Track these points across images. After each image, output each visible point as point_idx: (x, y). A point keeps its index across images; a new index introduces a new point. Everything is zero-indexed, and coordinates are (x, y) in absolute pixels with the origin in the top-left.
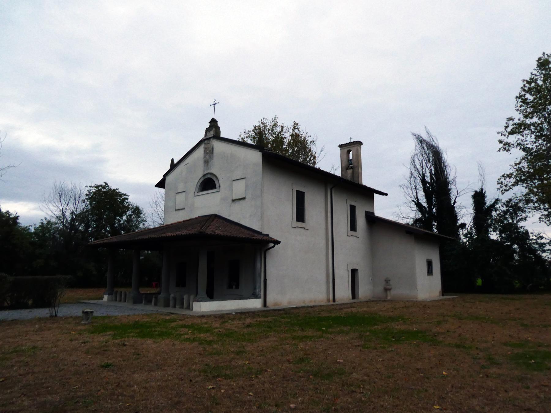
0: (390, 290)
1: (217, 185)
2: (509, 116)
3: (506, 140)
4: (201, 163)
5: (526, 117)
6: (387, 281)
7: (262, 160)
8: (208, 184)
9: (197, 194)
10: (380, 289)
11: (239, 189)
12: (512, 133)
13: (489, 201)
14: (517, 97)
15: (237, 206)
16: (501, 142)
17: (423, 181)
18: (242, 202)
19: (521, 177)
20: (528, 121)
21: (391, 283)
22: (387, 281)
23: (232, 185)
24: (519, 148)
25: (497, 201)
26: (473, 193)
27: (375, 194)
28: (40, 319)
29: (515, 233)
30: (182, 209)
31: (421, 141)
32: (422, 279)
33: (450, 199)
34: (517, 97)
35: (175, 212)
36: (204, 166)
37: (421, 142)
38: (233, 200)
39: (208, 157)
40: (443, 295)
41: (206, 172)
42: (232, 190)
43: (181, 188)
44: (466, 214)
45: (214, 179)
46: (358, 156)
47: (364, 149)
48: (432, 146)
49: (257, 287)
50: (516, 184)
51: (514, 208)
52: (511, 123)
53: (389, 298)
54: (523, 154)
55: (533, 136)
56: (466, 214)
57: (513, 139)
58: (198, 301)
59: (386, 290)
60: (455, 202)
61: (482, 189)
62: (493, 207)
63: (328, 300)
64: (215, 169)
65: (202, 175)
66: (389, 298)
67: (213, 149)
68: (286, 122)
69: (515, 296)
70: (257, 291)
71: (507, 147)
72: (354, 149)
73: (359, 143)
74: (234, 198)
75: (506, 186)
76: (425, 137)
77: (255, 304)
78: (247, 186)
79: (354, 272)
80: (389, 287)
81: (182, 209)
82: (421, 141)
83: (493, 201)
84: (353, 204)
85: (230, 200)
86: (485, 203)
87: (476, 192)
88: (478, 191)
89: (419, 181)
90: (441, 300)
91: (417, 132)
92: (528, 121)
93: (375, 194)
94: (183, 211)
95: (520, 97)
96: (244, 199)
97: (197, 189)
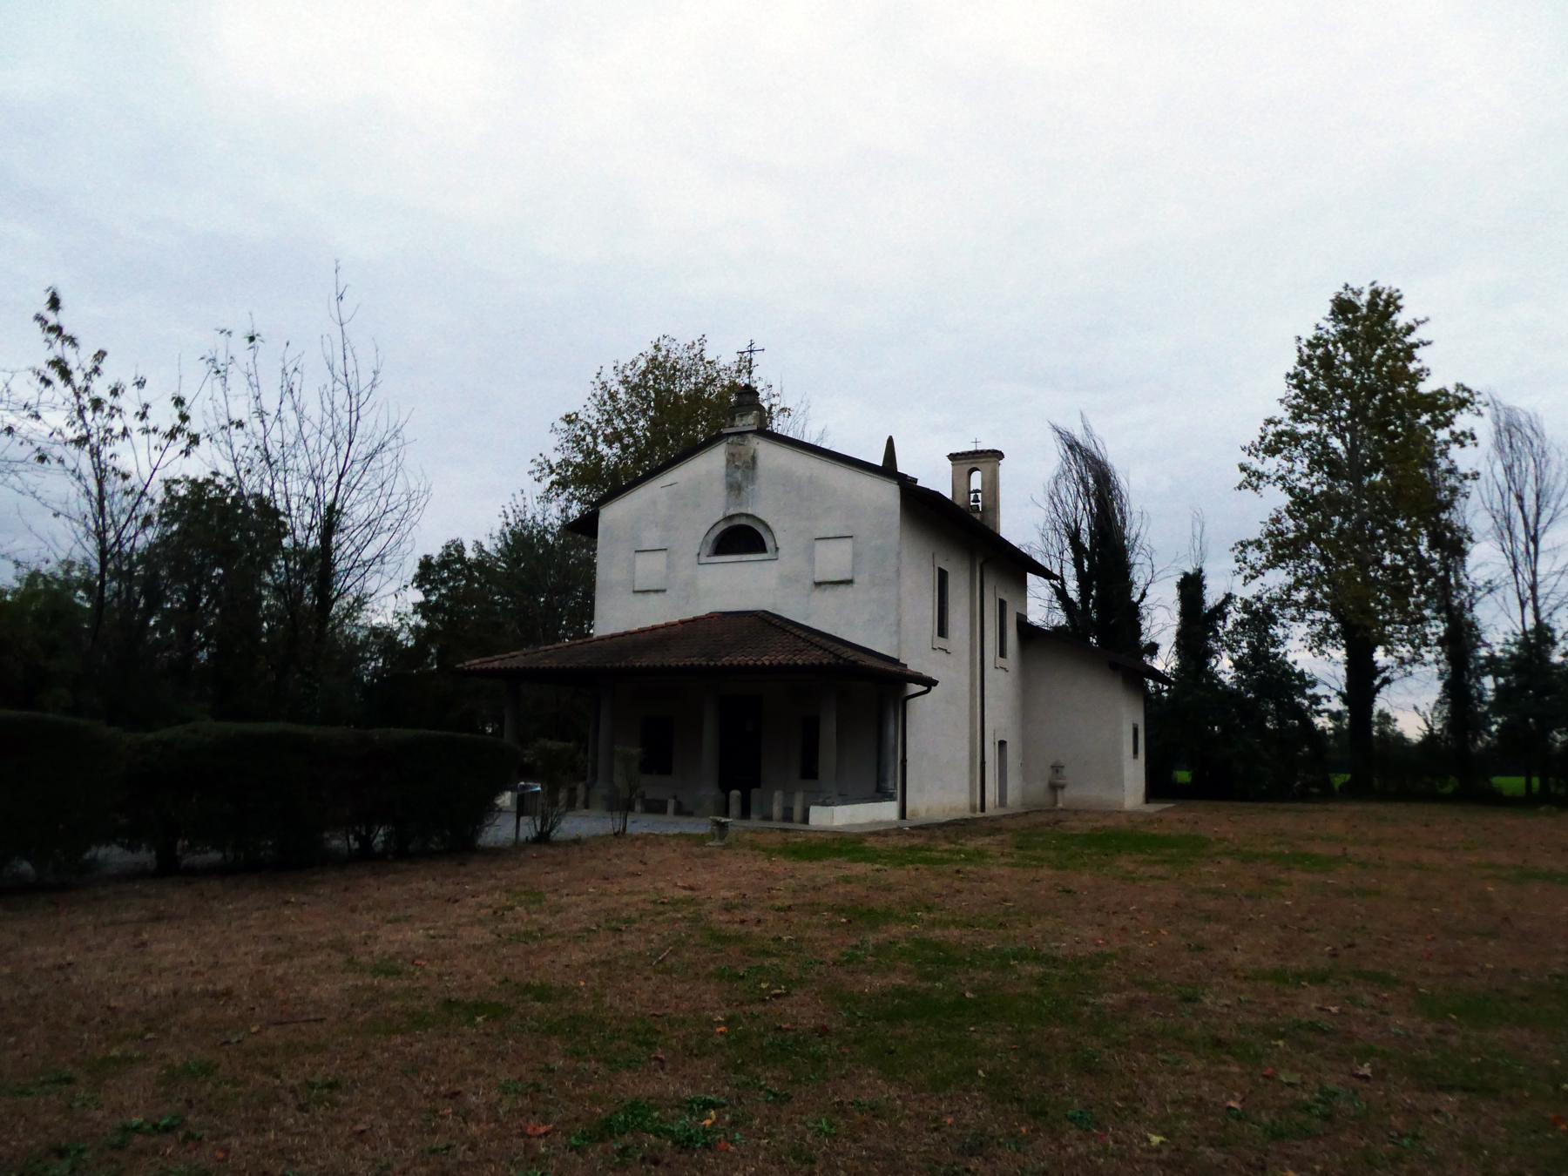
0: (1063, 787)
1: (769, 544)
2: (1268, 416)
3: (1255, 464)
4: (719, 488)
5: (1297, 417)
6: (1057, 768)
7: (898, 501)
8: (740, 538)
9: (704, 559)
10: (1039, 788)
11: (834, 560)
12: (1272, 450)
13: (1212, 597)
14: (1288, 375)
15: (830, 597)
16: (1243, 468)
17: (1074, 537)
18: (842, 588)
19: (1282, 549)
20: (1303, 429)
21: (1065, 772)
22: (1057, 768)
23: (813, 547)
24: (1279, 485)
25: (1229, 598)
26: (1179, 578)
27: (1029, 576)
28: (688, 837)
29: (209, 515)
30: (657, 591)
31: (1073, 446)
32: (1113, 765)
33: (1130, 585)
34: (1288, 375)
35: (632, 597)
36: (729, 495)
37: (1071, 447)
38: (818, 584)
39: (739, 475)
40: (1147, 802)
41: (732, 511)
42: (811, 560)
43: (651, 538)
44: (1161, 622)
45: (761, 530)
46: (992, 486)
47: (1004, 467)
48: (1093, 457)
49: (890, 775)
50: (1271, 565)
51: (1260, 619)
52: (1271, 429)
53: (1060, 805)
54: (1286, 499)
55: (1306, 461)
56: (1161, 622)
57: (1272, 465)
58: (824, 804)
59: (1054, 788)
60: (1143, 595)
61: (1201, 571)
62: (1220, 611)
63: (973, 809)
64: (763, 506)
65: (720, 516)
66: (1060, 805)
67: (754, 459)
68: (722, 353)
69: (1309, 806)
70: (890, 784)
71: (1252, 479)
72: (986, 466)
73: (998, 455)
74: (819, 579)
75: (1252, 567)
76: (1079, 435)
77: (887, 811)
78: (856, 555)
79: (1002, 744)
80: (1061, 782)
81: (657, 591)
82: (1073, 446)
83: (1222, 597)
84: (1005, 598)
85: (809, 583)
86: (1203, 602)
87: (1186, 574)
88: (1191, 572)
89: (1067, 542)
90: (1140, 813)
91: (1064, 425)
92: (1303, 429)
93: (1029, 576)
94: (661, 595)
95: (1295, 376)
96: (849, 582)
97: (708, 550)
